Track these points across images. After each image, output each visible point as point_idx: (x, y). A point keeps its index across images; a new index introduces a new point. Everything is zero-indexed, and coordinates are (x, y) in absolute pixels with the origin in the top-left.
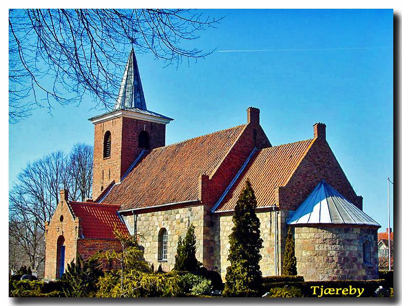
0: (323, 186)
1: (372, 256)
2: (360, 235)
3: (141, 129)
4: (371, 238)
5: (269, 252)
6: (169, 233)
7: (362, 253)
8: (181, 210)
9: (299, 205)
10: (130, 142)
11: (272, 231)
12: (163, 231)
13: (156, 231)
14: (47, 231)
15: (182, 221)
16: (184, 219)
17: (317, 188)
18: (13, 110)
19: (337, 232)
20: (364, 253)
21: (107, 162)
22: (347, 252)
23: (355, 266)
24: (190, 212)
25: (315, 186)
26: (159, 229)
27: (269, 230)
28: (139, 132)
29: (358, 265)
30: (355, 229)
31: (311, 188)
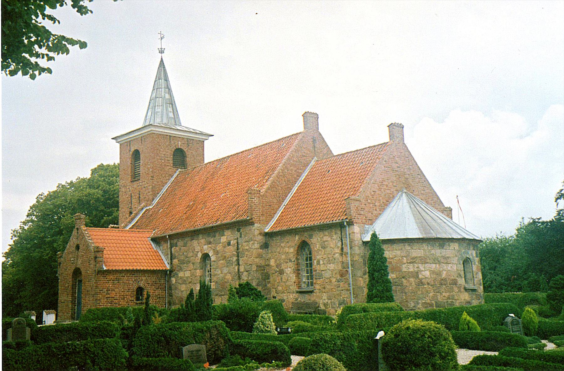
0: (404, 194)
1: (475, 276)
2: (459, 251)
3: (175, 146)
4: (472, 254)
5: (341, 276)
6: (213, 258)
7: (463, 272)
8: (228, 233)
9: (376, 219)
10: (163, 161)
11: (345, 250)
12: (206, 257)
13: (197, 258)
14: (60, 263)
15: (229, 244)
16: (232, 242)
17: (397, 198)
18: (8, 320)
19: (429, 248)
20: (465, 273)
21: (135, 185)
22: (445, 272)
23: (456, 289)
24: (239, 233)
25: (393, 196)
26: (200, 255)
27: (340, 248)
28: (173, 150)
29: (459, 288)
30: (451, 244)
31: (389, 198)
